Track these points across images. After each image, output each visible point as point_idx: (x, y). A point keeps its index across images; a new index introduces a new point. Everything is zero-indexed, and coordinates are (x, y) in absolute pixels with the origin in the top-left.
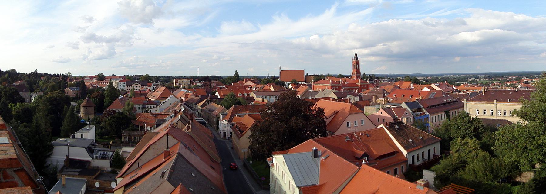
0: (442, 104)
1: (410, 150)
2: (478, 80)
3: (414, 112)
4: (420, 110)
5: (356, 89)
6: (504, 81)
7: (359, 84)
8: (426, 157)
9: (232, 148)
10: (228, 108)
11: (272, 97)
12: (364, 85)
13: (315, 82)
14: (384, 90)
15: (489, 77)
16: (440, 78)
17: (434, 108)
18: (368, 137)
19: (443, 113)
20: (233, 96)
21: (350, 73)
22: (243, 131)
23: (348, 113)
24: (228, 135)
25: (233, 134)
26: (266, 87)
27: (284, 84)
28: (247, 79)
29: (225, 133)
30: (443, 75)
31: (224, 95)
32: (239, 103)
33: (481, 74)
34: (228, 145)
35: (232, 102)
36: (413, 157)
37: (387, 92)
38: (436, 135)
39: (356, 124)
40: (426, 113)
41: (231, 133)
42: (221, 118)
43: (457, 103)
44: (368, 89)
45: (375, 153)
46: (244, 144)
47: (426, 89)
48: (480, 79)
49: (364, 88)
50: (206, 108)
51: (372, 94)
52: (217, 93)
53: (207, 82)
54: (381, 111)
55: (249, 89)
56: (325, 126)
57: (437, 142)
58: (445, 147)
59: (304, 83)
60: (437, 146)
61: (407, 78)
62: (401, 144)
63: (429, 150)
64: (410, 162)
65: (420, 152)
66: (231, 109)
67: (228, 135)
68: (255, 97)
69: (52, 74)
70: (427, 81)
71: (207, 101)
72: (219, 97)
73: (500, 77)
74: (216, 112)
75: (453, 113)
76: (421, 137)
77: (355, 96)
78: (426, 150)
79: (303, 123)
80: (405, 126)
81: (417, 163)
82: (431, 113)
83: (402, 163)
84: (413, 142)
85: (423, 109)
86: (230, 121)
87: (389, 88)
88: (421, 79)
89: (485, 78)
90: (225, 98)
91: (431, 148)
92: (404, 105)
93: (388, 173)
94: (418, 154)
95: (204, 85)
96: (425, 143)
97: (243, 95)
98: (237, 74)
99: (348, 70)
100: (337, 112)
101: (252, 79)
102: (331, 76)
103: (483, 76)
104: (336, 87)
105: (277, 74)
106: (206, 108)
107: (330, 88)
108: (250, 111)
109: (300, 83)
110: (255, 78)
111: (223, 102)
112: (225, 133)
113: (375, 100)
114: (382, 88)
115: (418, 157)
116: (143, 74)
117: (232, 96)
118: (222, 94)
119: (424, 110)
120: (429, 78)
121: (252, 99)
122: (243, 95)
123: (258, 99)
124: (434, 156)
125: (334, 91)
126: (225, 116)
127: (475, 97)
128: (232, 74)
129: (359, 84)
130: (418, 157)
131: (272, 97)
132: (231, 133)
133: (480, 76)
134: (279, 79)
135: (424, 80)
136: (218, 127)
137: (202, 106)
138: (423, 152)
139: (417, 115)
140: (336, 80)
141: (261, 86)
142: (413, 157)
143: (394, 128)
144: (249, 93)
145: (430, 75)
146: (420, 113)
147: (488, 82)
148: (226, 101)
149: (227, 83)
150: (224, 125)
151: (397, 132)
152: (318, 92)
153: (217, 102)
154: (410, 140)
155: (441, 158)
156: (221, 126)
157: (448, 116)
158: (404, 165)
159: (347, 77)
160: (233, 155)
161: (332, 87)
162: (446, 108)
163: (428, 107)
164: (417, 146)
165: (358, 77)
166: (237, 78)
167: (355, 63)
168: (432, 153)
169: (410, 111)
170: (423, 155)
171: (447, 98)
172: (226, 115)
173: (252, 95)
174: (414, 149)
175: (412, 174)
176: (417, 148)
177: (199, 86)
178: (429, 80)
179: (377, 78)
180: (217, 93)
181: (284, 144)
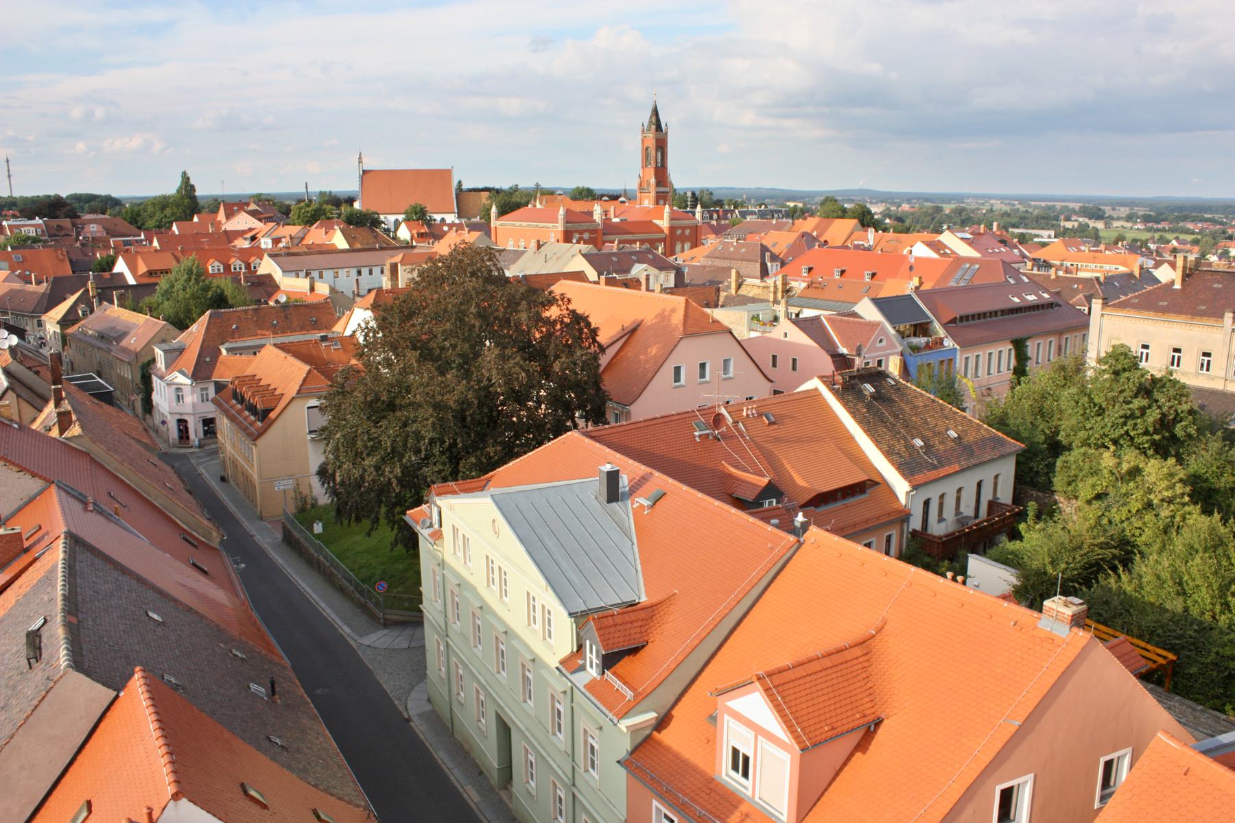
0: (1003, 312)
1: (920, 478)
2: (1100, 225)
3: (902, 335)
4: (922, 329)
5: (653, 243)
6: (1214, 236)
7: (664, 223)
8: (968, 509)
9: (223, 479)
10: (181, 324)
11: (342, 273)
12: (684, 228)
14: (764, 249)
15: (1146, 219)
16: (947, 208)
17: (973, 324)
18: (771, 423)
19: (1007, 348)
20: (196, 275)
21: (633, 185)
22: (267, 412)
23: (679, 333)
24: (195, 431)
25: (223, 424)
26: (316, 235)
27: (376, 223)
28: (234, 206)
29: (182, 423)
30: (959, 198)
31: (150, 273)
32: (220, 301)
33: (1116, 203)
34: (201, 470)
35: (194, 296)
36: (927, 503)
37: (774, 258)
38: (1001, 422)
39: (703, 375)
40: (949, 343)
41: (209, 423)
42: (161, 364)
43: (1058, 314)
44: (696, 243)
45: (800, 482)
46: (292, 456)
47: (921, 250)
48: (1108, 220)
49: (683, 239)
50: (89, 326)
51: (726, 263)
52: (120, 266)
53: (66, 222)
54: (785, 326)
55: (246, 244)
56: (596, 381)
57: (1009, 455)
58: (1036, 470)
59: (451, 218)
60: (1007, 470)
61: (833, 208)
62: (889, 454)
63: (979, 485)
64: (916, 523)
65: (949, 488)
66: (198, 329)
67: (195, 431)
68: (278, 274)
70: (900, 219)
71: (84, 299)
72: (131, 281)
73: (1194, 220)
74: (133, 342)
75: (1041, 351)
76: (953, 434)
77: (661, 268)
78: (968, 483)
79: (527, 372)
80: (897, 388)
81: (937, 529)
82: (965, 344)
83: (891, 523)
84: (927, 447)
85: (937, 326)
86: (201, 373)
87: (780, 239)
88: (877, 209)
89: (1129, 218)
90: (163, 283)
91: (986, 474)
92: (868, 311)
93: (868, 545)
94: (942, 497)
95: (55, 234)
96: (969, 454)
97: (227, 267)
98: (187, 187)
99: (623, 171)
100: (633, 331)
101: (253, 207)
102: (551, 193)
103: (1124, 211)
104: (581, 232)
105: (347, 184)
106: (89, 326)
107: (561, 237)
108: (276, 330)
109: (438, 217)
110: (259, 199)
111: (155, 298)
112: (182, 423)
113: (739, 286)
114: (756, 239)
115: (941, 505)
117: (190, 272)
118: (142, 269)
119: (941, 332)
120: (906, 207)
121: (267, 285)
122: (227, 267)
123: (291, 285)
124: (993, 505)
125: (584, 248)
126: (175, 355)
127: (1124, 292)
128: (170, 187)
129: (664, 223)
130: (941, 505)
131: (342, 273)
132: (209, 423)
133: (1108, 211)
134: (357, 205)
135: (887, 214)
136: (148, 405)
137: (65, 322)
138: (959, 490)
139: (915, 349)
141: (294, 230)
142: (927, 503)
143: (860, 394)
144: (254, 261)
145: (909, 198)
146: (922, 340)
147: (1145, 236)
148: (167, 294)
149: (151, 223)
150: (176, 395)
151: (869, 407)
152: (518, 254)
153: (129, 302)
154: (918, 442)
155: (1022, 516)
156: (162, 398)
157: (1022, 358)
158: (894, 533)
159: (614, 197)
160: (232, 508)
161: (567, 237)
162: (1018, 327)
163: (953, 321)
164: (941, 464)
165: (661, 198)
166: (187, 203)
167: (652, 144)
168: (986, 496)
169: (892, 331)
170: (958, 500)
171: (1020, 288)
172: (181, 350)
173: (267, 266)
174: (932, 474)
175: (939, 553)
176: (942, 472)
177: (35, 240)
178: (929, 218)
179: (719, 203)
180: (120, 266)
181: (481, 442)
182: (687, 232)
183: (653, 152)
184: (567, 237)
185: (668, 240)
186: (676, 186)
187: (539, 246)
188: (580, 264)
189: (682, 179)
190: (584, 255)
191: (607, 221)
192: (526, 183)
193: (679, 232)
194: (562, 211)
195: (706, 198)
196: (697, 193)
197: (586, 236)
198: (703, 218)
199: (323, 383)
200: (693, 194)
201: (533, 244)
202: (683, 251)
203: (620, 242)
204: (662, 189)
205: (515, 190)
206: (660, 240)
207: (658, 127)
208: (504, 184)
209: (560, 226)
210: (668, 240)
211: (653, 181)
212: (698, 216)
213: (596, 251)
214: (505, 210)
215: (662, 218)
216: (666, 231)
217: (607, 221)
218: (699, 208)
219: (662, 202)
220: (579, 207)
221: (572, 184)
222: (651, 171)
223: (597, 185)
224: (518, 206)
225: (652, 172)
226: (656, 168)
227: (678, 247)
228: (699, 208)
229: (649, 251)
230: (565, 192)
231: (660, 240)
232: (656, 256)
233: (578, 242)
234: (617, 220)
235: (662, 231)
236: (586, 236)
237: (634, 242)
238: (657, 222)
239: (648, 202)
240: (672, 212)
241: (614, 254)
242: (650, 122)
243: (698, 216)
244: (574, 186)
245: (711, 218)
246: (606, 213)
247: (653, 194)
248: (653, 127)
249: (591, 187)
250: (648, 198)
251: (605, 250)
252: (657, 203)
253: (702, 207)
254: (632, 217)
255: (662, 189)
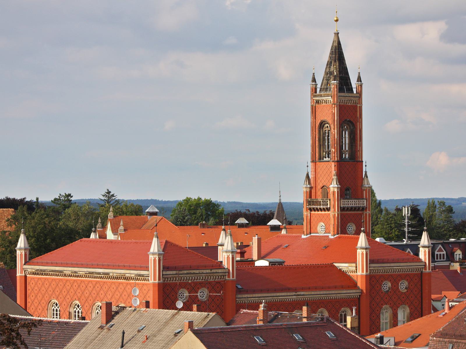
5: (336, 308)
7: (357, 269)
12: (395, 279)
13: (37, 251)
21: (296, 195)
44: (420, 308)
49: (395, 300)
69: (16, 199)
99: (274, 167)
102: (136, 210)
104: (193, 287)
107: (152, 296)
116: (94, 199)
125: (196, 316)
128: (30, 200)
129: (357, 269)
140: (189, 237)
159: (258, 218)
161: (166, 297)
165: (350, 219)
167: (329, 113)
182: (403, 286)
183: (334, 132)
184: (166, 297)
185: (365, 304)
186: (379, 197)
187: (110, 315)
188: (388, 307)
189: (389, 184)
190: (197, 333)
191: (244, 263)
192: (86, 192)
193: (387, 285)
194: (155, 247)
195: (439, 219)
196: (423, 209)
197: (203, 294)
198: (433, 256)
199: (188, 200)
200: (415, 211)
201: (97, 315)
202: (394, 323)
203: (270, 306)
204: (351, 203)
205: (65, 203)
206: (349, 303)
207: (344, 83)
208: (43, 192)
209: (152, 276)
210: (365, 304)
211: (334, 187)
212: (423, 255)
213: (221, 325)
214: (38, 249)
215: (353, 260)
216: (361, 284)
217: (244, 263)
218: (425, 240)
219: (351, 227)
220: (189, 237)
221: (175, 194)
222: (329, 171)
223: (223, 196)
224: (70, 236)
225: (332, 168)
226: (341, 163)
227: (386, 316)
228: (425, 240)
229: (326, 324)
230: (164, 209)
231: (349, 303)
232: (341, 333)
233: (187, 307)
234: (264, 263)
235: (354, 285)
236: (203, 294)
237: (297, 305)
238: (343, 266)
239: (324, 227)
240: (372, 247)
241: (257, 331)
242: (328, 74)
243: (423, 255)
244: (181, 198)
245: (450, 258)
246: (242, 249)
247: (333, 213)
248: (334, 83)
249: (215, 199)
250: (326, 220)
251: (240, 324)
252: (342, 229)
253: (431, 237)
254: (292, 258)
255: (351, 203)
